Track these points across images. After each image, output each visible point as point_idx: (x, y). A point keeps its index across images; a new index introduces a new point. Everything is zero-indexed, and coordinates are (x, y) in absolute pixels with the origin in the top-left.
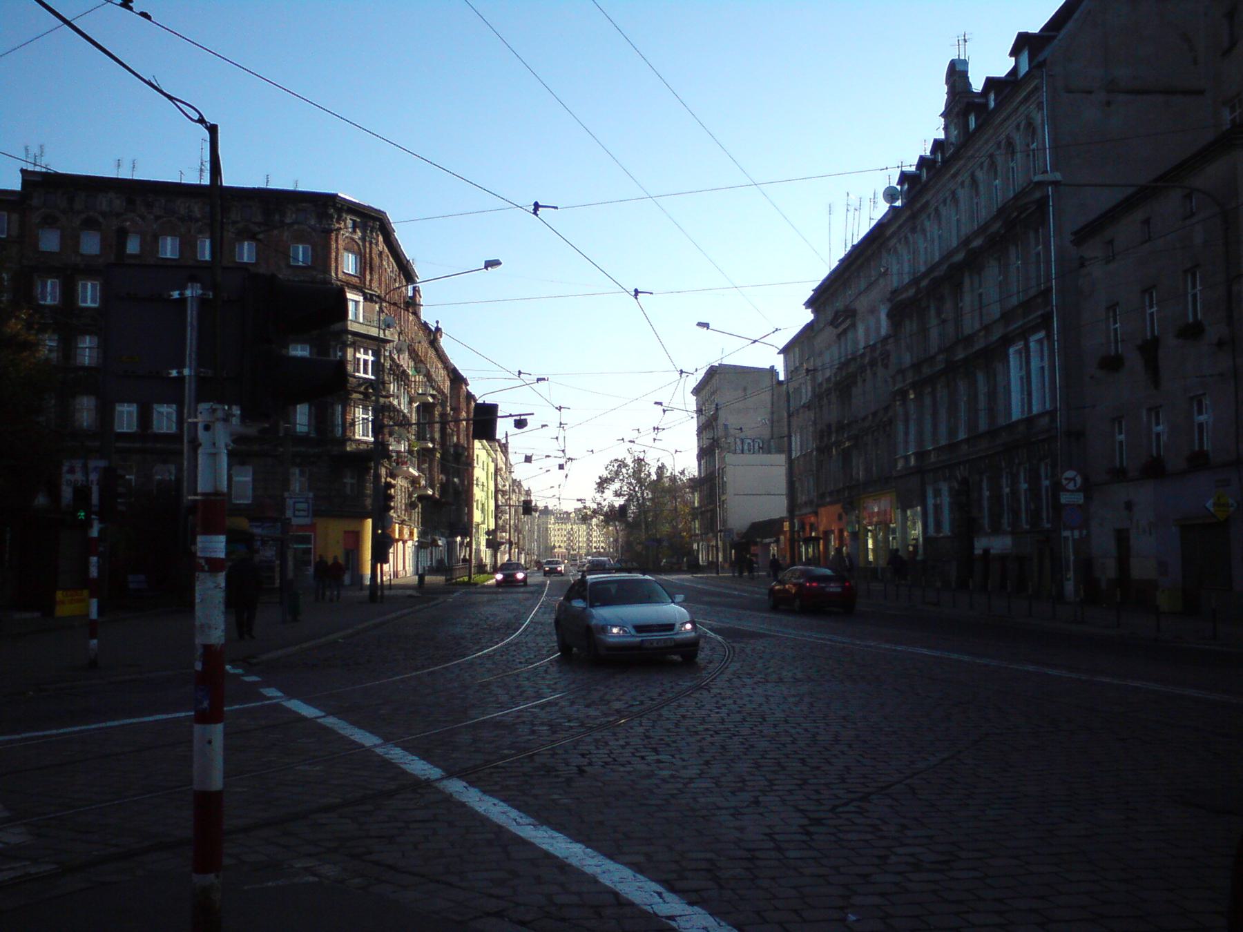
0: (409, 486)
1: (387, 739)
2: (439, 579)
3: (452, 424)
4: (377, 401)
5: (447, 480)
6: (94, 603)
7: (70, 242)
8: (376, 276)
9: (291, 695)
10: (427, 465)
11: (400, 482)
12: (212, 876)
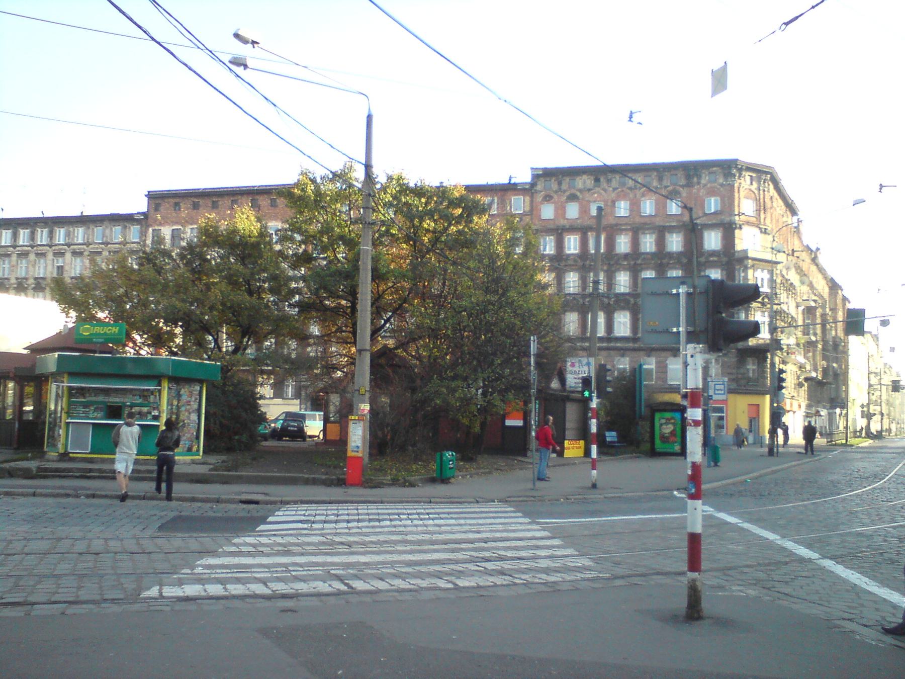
0: (797, 370)
1: (783, 537)
4: (772, 308)
5: (828, 365)
7: (561, 210)
8: (768, 215)
12: (697, 573)
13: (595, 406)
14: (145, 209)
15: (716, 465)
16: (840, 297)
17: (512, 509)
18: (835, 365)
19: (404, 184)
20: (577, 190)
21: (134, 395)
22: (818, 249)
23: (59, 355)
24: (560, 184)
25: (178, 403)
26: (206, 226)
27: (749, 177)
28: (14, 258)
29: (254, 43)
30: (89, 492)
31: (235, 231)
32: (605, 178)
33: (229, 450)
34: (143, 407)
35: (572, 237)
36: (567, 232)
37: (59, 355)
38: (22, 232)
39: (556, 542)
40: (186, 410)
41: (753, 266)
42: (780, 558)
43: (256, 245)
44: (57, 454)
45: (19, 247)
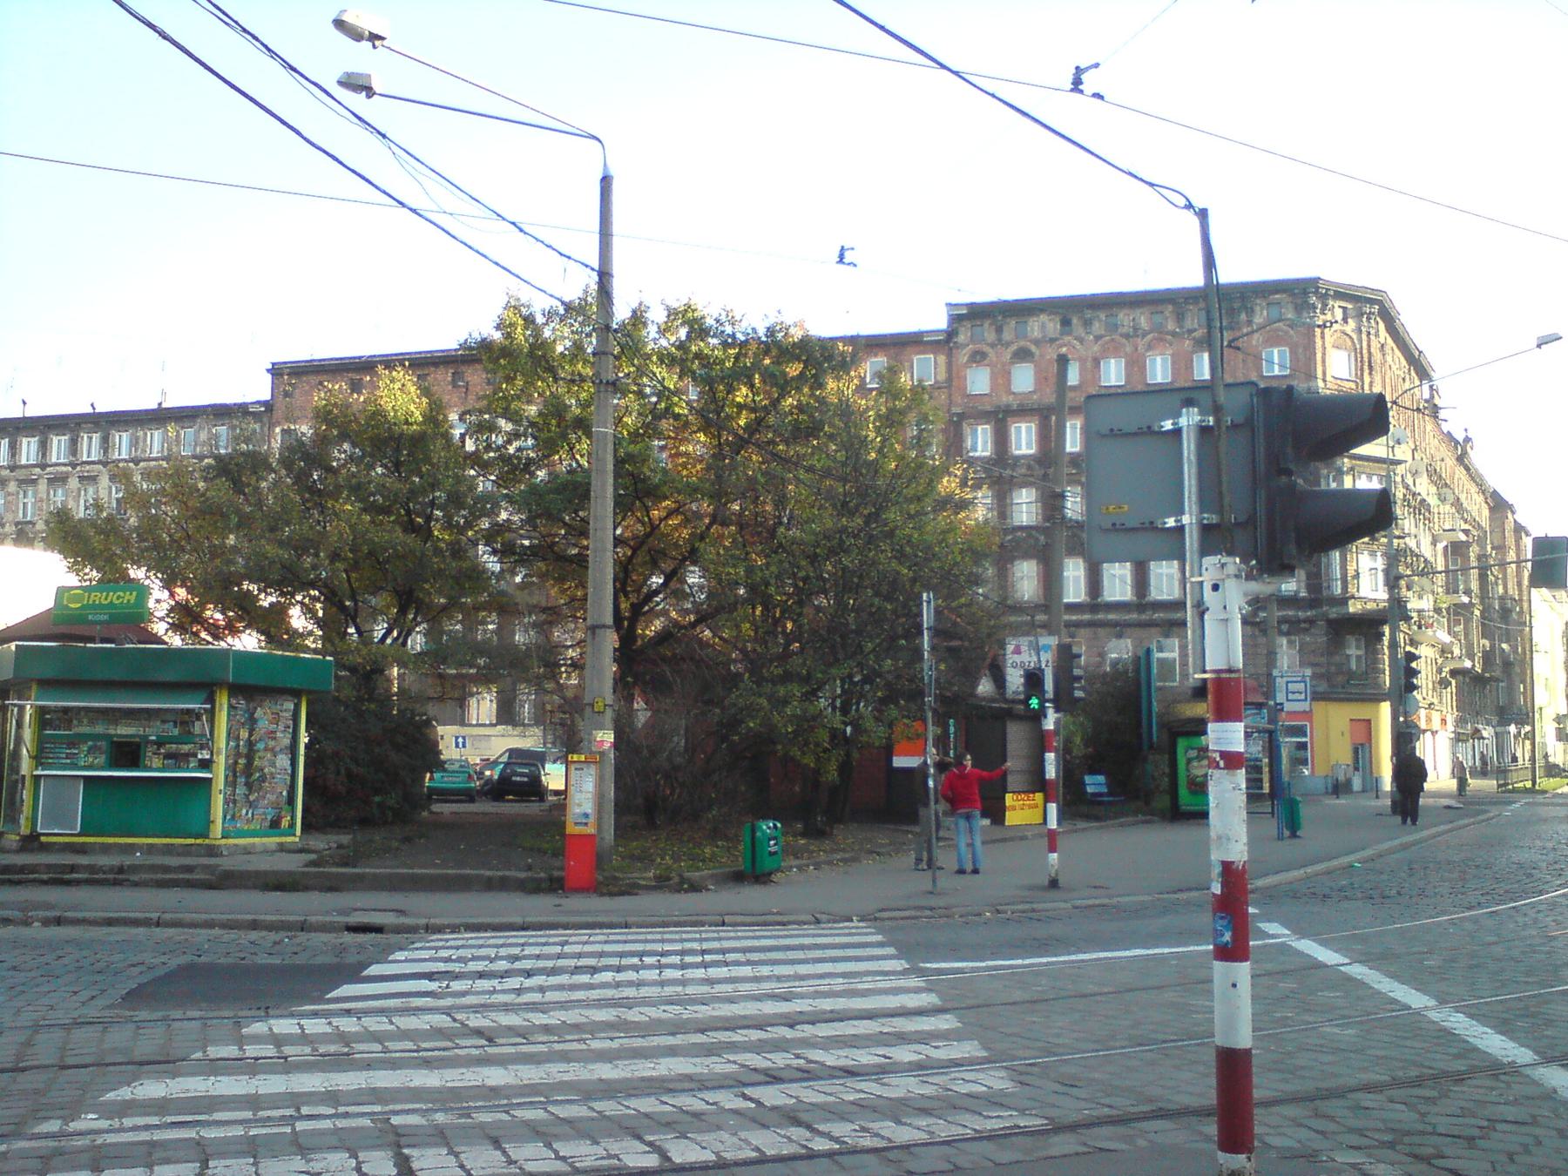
0: (1438, 657)
1: (1442, 1001)
2: (1489, 784)
3: (1495, 570)
5: (1493, 646)
6: (1053, 808)
7: (1002, 378)
9: (1302, 934)
10: (1462, 626)
11: (1425, 652)
13: (1052, 727)
14: (267, 396)
15: (1294, 835)
16: (1510, 525)
17: (879, 938)
18: (1504, 646)
19: (695, 320)
20: (1031, 341)
21: (164, 722)
22: (1467, 440)
23: (17, 646)
24: (999, 330)
25: (251, 735)
26: (326, 405)
27: (1341, 310)
28: (42, 486)
29: (374, 37)
30: (50, 914)
31: (379, 414)
32: (1080, 318)
33: (365, 822)
34: (181, 744)
35: (1023, 426)
36: (1013, 416)
37: (17, 646)
38: (55, 440)
39: (946, 1022)
40: (266, 749)
41: (1352, 469)
42: (1442, 1063)
43: (418, 441)
44: (18, 838)
45: (51, 466)
